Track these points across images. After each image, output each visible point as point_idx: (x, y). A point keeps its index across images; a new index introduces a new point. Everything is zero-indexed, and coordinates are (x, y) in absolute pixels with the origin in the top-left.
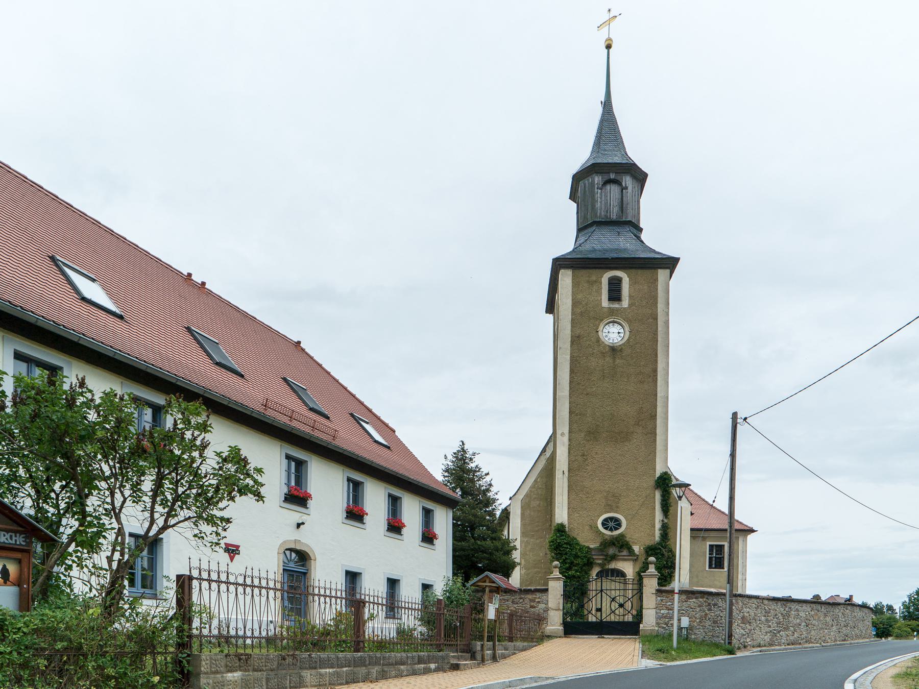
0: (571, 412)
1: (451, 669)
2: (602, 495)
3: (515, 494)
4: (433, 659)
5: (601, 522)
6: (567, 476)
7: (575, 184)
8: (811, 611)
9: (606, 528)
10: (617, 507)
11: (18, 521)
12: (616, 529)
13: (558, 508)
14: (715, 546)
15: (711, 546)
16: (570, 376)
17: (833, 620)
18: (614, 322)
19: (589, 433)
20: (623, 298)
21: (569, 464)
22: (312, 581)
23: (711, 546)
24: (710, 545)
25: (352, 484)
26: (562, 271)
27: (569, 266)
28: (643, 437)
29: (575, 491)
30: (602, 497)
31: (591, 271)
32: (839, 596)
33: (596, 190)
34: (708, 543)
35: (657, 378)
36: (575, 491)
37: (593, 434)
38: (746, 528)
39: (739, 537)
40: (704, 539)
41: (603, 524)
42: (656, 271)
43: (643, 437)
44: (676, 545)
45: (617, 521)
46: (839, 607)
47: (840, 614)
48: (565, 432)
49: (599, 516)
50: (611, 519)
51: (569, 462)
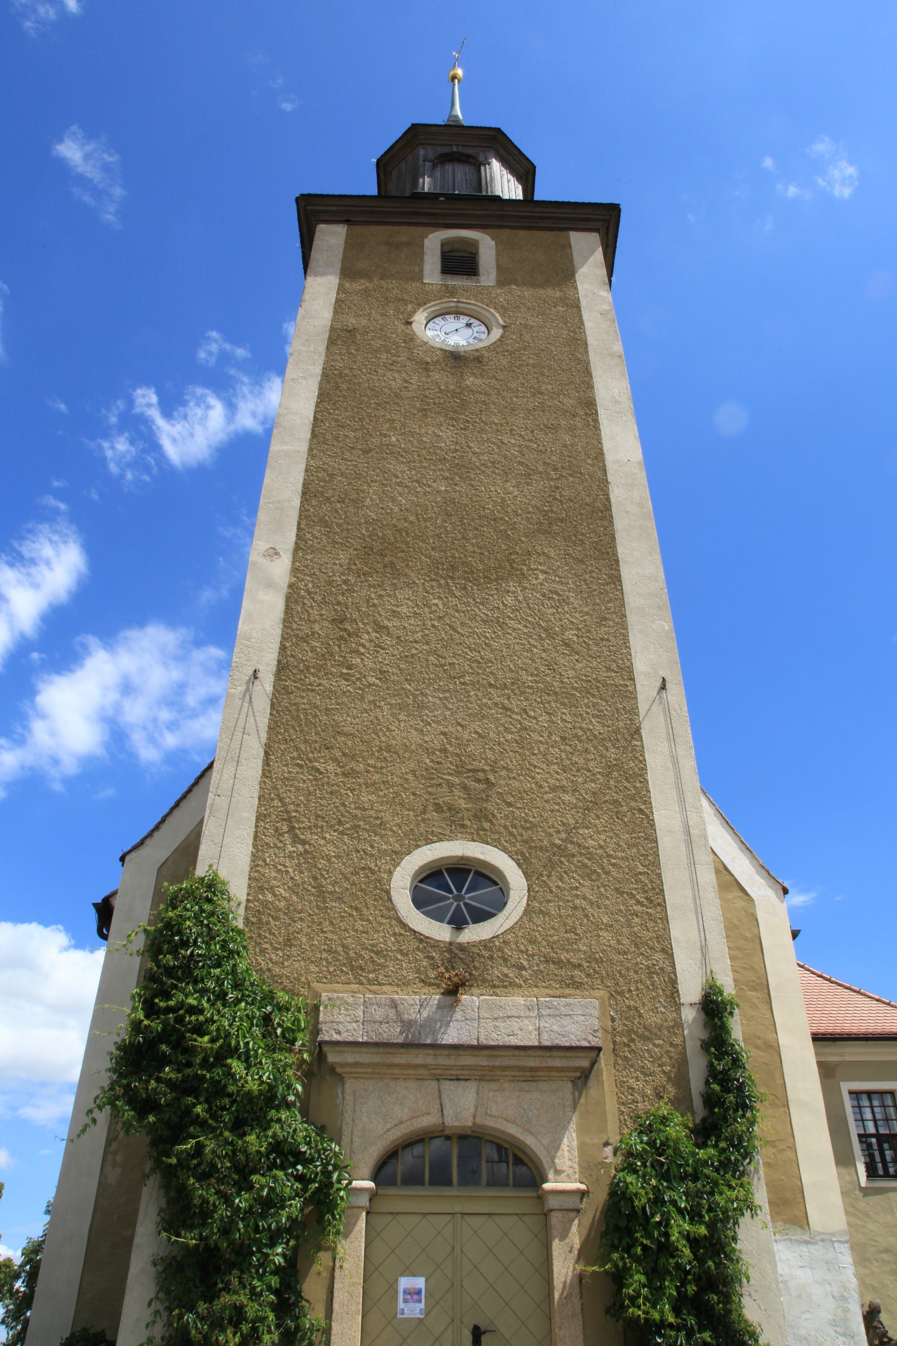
0: (307, 493)
1: (711, 987)
2: (412, 765)
3: (142, 842)
6: (269, 688)
7: (382, 174)
13: (529, 1131)
14: (489, 1151)
16: (317, 406)
18: (458, 313)
19: (367, 551)
20: (482, 270)
21: (283, 648)
26: (321, 228)
27: (522, 1079)
28: (572, 568)
29: (297, 749)
30: (413, 772)
31: (395, 228)
33: (421, 162)
35: (596, 421)
36: (297, 749)
37: (332, 343)
41: (420, 901)
42: (564, 233)
43: (572, 568)
48: (278, 548)
49: (397, 857)
51: (284, 638)
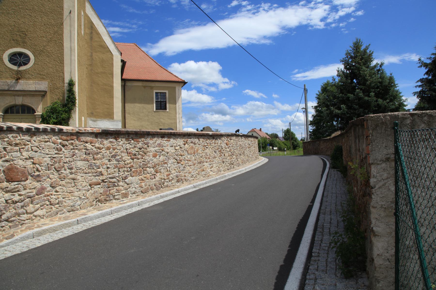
4: (83, 207)
5: (30, 62)
8: (185, 145)
9: (15, 64)
10: (24, 42)
11: (16, 93)
12: (25, 64)
15: (156, 93)
17: (215, 152)
22: (162, 131)
23: (156, 93)
24: (166, 93)
25: (247, 91)
32: (255, 129)
34: (155, 91)
38: (180, 80)
39: (175, 87)
40: (152, 88)
44: (78, 84)
45: (27, 59)
46: (223, 139)
47: (223, 145)
49: (4, 51)
50: (20, 54)
